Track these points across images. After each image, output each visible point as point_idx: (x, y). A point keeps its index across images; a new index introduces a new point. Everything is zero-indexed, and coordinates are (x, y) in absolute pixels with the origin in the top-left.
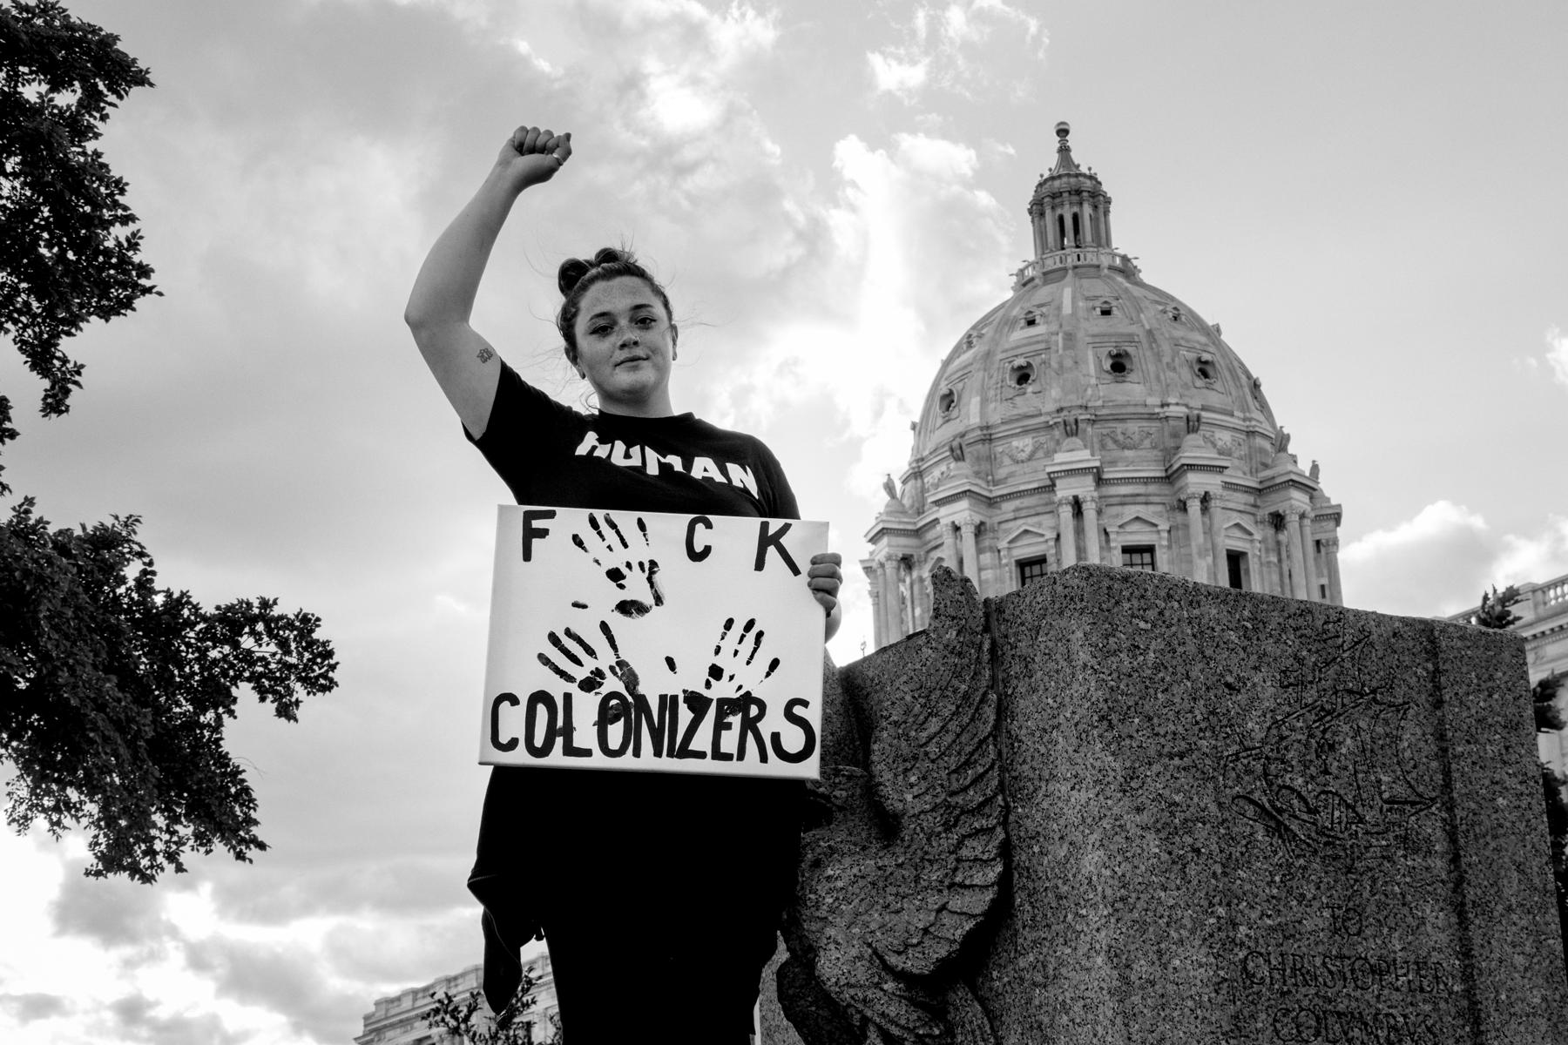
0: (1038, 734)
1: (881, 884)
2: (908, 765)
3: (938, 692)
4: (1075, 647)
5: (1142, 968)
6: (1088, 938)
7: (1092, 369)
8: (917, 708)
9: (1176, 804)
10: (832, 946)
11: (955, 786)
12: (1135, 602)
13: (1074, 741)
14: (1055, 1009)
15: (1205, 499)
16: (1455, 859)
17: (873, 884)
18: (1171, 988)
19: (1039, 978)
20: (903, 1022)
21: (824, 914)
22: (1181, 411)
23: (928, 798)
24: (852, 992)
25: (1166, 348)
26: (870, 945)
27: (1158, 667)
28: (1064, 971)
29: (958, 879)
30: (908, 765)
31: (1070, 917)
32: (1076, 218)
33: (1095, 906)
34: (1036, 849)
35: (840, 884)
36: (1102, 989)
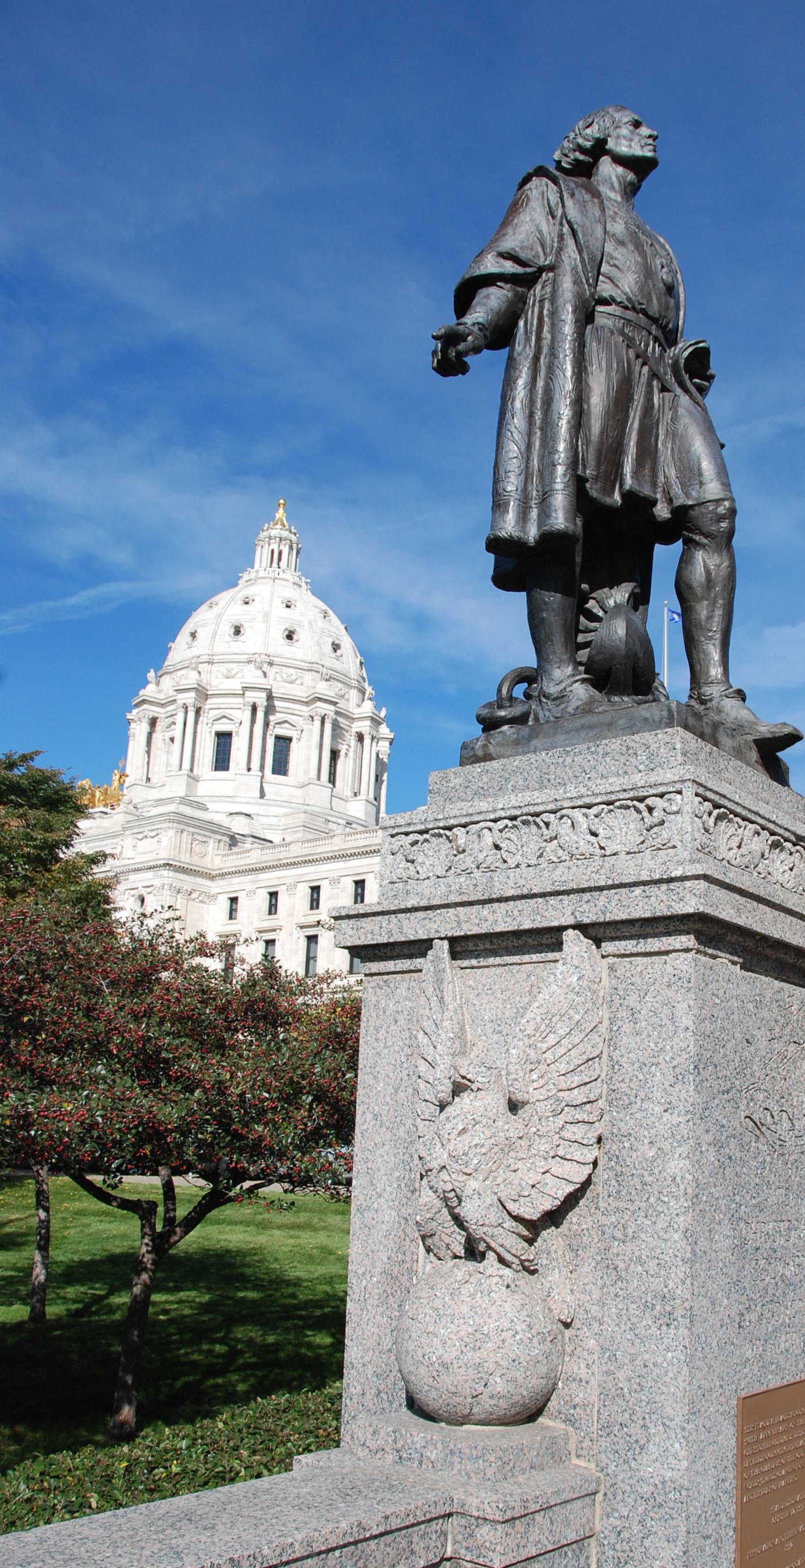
1: (506, 1150)
3: (558, 1017)
4: (678, 1013)
5: (703, 1244)
6: (668, 1219)
8: (543, 1027)
9: (723, 1126)
10: (476, 1196)
11: (563, 1086)
13: (672, 1080)
14: (631, 1259)
19: (619, 1235)
20: (514, 1252)
23: (543, 1091)
26: (496, 1193)
28: (642, 1236)
29: (561, 1153)
31: (652, 1200)
32: (280, 553)
33: (677, 1198)
34: (627, 1145)
36: (676, 1256)
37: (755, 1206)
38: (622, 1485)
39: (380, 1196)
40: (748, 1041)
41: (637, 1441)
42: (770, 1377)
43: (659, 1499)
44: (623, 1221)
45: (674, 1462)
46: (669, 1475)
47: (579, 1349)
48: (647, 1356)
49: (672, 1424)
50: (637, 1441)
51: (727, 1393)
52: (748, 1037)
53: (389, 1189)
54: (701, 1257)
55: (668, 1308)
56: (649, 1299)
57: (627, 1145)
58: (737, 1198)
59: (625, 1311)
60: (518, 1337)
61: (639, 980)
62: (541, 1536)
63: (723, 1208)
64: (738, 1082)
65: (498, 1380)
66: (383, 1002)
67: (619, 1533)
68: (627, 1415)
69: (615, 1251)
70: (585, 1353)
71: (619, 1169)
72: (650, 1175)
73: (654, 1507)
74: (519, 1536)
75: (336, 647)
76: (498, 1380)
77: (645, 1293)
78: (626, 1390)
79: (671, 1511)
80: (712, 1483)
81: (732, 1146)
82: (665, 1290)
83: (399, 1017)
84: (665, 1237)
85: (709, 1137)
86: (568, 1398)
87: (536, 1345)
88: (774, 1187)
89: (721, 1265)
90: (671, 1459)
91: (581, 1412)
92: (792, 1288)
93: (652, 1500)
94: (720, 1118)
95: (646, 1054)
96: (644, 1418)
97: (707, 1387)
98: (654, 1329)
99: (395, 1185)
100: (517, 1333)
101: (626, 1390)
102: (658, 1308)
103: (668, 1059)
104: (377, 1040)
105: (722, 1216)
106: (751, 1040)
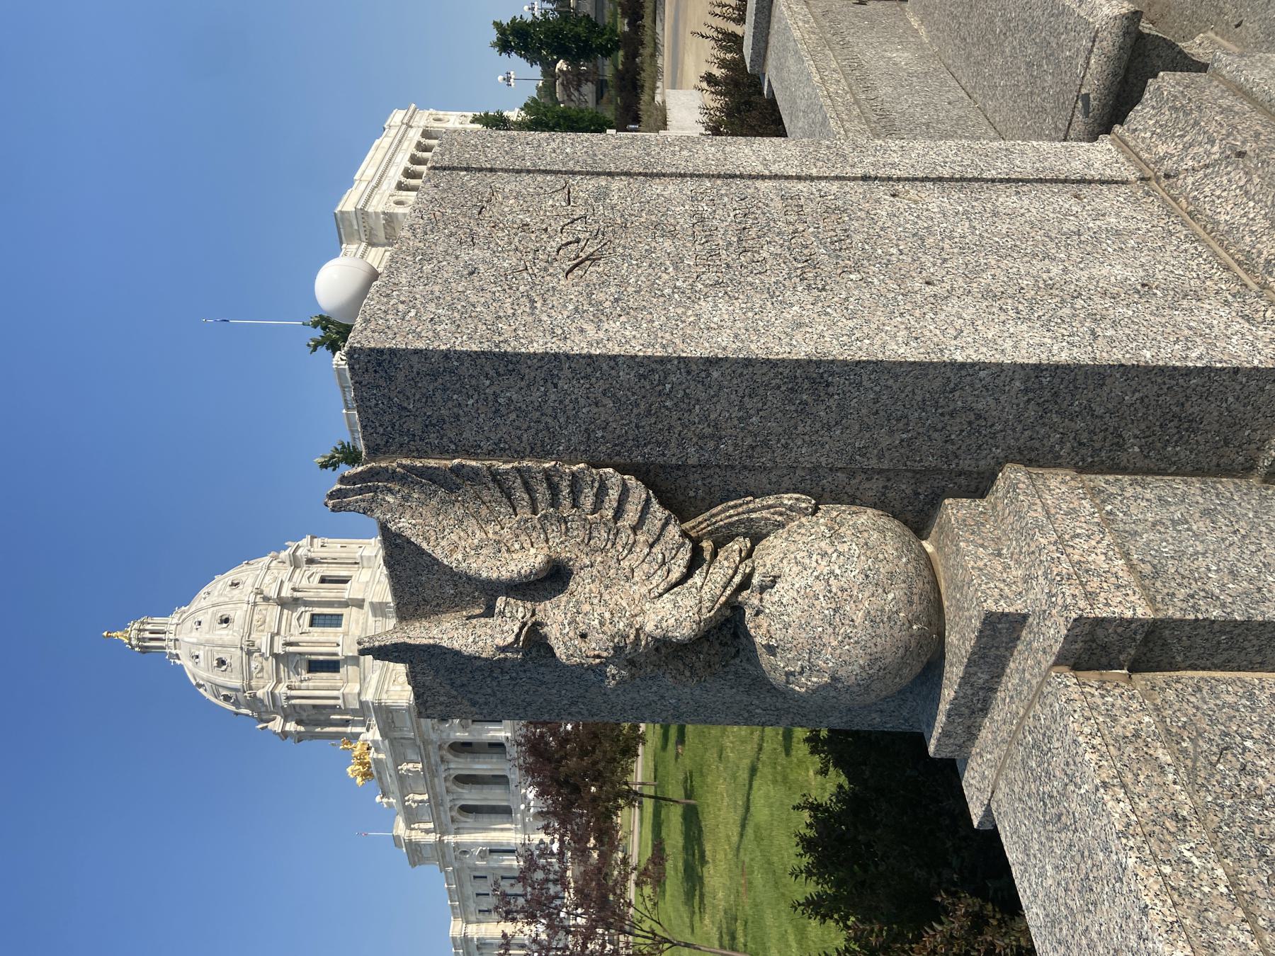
0: (498, 420)
2: (504, 549)
7: (225, 632)
9: (576, 309)
12: (389, 317)
14: (743, 429)
15: (294, 589)
16: (610, 174)
17: (607, 587)
18: (738, 324)
19: (711, 444)
20: (731, 572)
21: (633, 631)
22: (252, 596)
24: (704, 610)
25: (222, 599)
27: (451, 307)
30: (504, 549)
34: (600, 434)
35: (607, 615)
37: (676, 268)
38: (1022, 441)
39: (663, 697)
40: (471, 273)
41: (970, 423)
42: (880, 251)
43: (1047, 395)
44: (695, 440)
45: (1002, 378)
46: (1018, 384)
47: (848, 489)
48: (864, 411)
49: (954, 380)
50: (970, 423)
51: (909, 306)
52: (465, 272)
53: (655, 688)
54: (743, 341)
55: (806, 385)
56: (793, 408)
57: (600, 434)
58: (666, 291)
59: (807, 438)
60: (838, 571)
61: (387, 418)
62: (1098, 551)
63: (680, 311)
64: (522, 288)
65: (891, 596)
66: (442, 699)
67: (1080, 444)
68: (936, 435)
69: (731, 449)
70: (853, 482)
71: (631, 443)
72: (638, 405)
73: (1056, 403)
74: (1105, 585)
75: (235, 585)
76: (891, 596)
77: (785, 413)
78: (904, 436)
79: (1065, 383)
80: (1024, 327)
81: (602, 297)
82: (783, 388)
83: (458, 682)
84: (716, 388)
85: (590, 329)
86: (906, 502)
87: (845, 547)
88: (653, 244)
89: (750, 314)
90: (999, 382)
91: (923, 487)
92: (772, 224)
93: (1047, 405)
94: (566, 313)
95: (483, 409)
96: (942, 415)
97: (904, 333)
98: (831, 402)
99: (650, 682)
100: (832, 572)
101: (904, 436)
102: (805, 397)
103: (488, 382)
104: (486, 704)
105: (690, 312)
106: (470, 268)
